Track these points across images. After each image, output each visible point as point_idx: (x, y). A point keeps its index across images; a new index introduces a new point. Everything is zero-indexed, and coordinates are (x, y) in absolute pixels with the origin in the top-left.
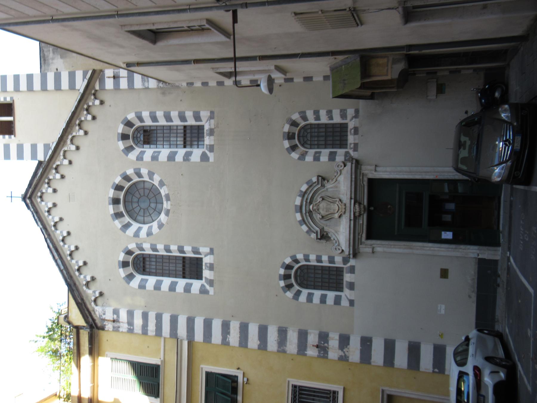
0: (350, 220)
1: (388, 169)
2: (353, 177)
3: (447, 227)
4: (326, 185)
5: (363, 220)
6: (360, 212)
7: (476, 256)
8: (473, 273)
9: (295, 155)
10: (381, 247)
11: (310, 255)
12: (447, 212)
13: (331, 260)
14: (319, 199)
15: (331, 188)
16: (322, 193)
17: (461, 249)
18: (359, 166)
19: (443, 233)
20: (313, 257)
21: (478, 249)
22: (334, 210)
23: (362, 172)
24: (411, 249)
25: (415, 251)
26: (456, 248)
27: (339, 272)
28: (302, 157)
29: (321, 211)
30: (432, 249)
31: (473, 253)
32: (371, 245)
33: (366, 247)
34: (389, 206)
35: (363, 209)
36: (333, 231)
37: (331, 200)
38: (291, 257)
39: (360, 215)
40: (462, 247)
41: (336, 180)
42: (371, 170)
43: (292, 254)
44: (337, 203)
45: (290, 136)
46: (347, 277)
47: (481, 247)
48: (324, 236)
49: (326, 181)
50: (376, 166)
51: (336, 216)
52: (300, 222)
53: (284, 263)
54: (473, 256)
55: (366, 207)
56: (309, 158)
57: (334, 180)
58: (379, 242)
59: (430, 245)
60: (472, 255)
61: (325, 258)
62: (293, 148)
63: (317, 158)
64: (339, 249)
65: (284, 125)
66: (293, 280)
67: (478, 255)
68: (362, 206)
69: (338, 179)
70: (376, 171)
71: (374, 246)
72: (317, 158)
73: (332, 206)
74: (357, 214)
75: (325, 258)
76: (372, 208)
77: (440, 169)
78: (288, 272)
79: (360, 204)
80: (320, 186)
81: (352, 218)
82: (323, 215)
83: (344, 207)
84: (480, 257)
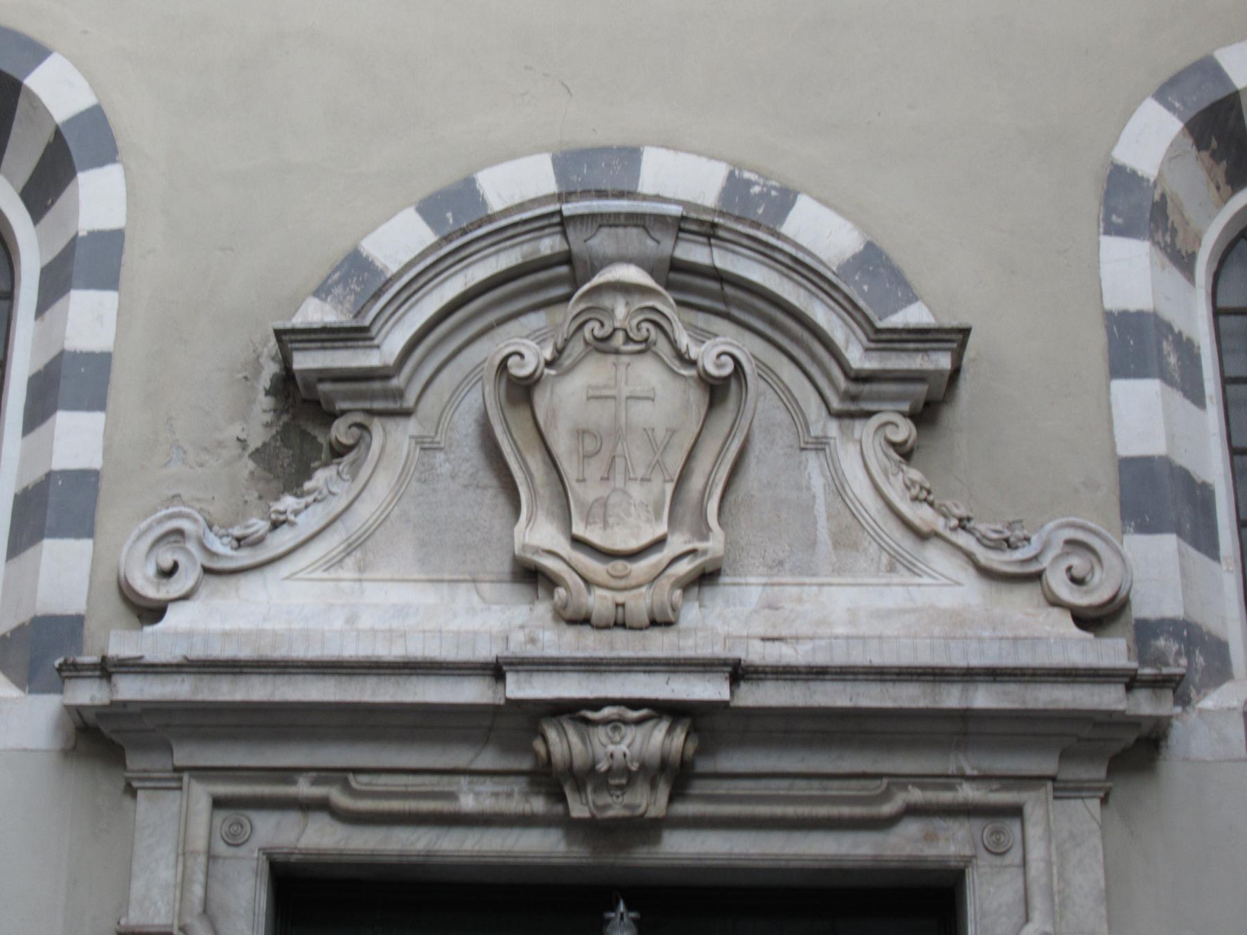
0: (496, 671)
2: (983, 698)
4: (865, 430)
6: (587, 777)
9: (1151, 139)
11: (108, 300)
15: (839, 488)
16: (784, 390)
23: (1035, 803)
28: (1133, 206)
33: (184, 853)
35: (616, 806)
36: (366, 511)
37: (709, 472)
38: (94, 119)
39: (550, 779)
41: (922, 536)
43: (122, 122)
44: (677, 544)
48: (311, 413)
49: (904, 431)
51: (539, 535)
55: (643, 856)
56: (1131, 273)
57: (922, 515)
64: (168, 573)
69: (935, 555)
72: (1136, 344)
74: (563, 743)
79: (678, 776)
80: (857, 358)
81: (519, 688)
82: (542, 400)
83: (640, 603)
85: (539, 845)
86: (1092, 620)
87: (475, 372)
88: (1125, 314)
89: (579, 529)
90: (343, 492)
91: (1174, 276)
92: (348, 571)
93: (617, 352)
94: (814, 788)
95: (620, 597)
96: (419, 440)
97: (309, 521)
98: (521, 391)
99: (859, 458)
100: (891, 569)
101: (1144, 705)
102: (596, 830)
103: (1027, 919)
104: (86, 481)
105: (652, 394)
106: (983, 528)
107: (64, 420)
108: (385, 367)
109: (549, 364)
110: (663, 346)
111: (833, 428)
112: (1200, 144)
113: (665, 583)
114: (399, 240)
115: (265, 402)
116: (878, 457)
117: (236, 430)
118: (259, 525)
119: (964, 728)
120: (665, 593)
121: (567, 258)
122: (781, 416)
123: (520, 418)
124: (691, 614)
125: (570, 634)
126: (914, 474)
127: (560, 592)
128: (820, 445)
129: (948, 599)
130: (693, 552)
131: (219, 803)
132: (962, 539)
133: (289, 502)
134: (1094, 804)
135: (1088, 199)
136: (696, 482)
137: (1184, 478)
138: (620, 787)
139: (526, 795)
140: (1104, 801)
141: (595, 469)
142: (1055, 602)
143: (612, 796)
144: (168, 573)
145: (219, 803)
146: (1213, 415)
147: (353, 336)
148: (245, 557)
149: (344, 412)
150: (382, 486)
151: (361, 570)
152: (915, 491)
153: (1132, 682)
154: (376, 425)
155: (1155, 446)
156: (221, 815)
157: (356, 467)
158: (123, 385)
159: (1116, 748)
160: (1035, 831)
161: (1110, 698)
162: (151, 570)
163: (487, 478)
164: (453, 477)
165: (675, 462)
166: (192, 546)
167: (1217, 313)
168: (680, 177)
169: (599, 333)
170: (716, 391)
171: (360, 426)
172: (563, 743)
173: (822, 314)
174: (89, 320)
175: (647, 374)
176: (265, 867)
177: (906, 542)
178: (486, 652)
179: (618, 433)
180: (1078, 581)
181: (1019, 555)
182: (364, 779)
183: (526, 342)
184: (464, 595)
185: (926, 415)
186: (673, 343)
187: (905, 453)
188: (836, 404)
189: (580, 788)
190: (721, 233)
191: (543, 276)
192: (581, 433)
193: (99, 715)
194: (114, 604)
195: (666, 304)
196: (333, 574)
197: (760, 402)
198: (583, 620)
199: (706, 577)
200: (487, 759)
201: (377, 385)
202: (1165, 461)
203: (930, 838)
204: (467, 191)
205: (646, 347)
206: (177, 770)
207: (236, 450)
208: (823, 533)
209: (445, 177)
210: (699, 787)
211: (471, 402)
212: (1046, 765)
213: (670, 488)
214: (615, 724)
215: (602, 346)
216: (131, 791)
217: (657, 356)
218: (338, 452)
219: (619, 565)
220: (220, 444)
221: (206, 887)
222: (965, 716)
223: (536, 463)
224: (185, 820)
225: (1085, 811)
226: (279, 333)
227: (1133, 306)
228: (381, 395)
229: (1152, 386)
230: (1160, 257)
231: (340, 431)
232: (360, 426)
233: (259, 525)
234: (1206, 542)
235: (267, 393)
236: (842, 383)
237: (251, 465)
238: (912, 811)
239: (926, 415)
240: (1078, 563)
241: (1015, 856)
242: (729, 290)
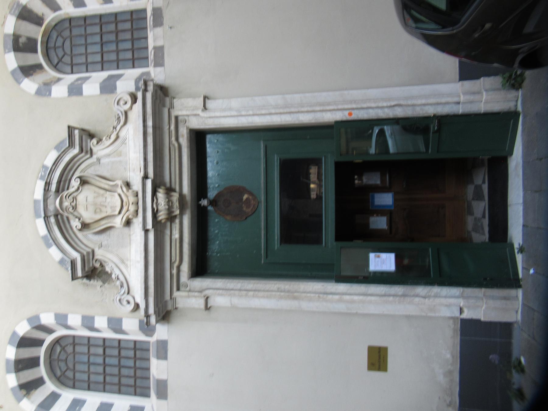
0: (146, 231)
1: (235, 103)
2: (150, 123)
3: (380, 241)
4: (95, 150)
5: (183, 230)
6: (170, 210)
7: (457, 314)
8: (449, 356)
9: (30, 85)
10: (225, 293)
11: (70, 316)
12: (381, 211)
13: (115, 324)
14: (75, 183)
15: (108, 155)
16: (87, 168)
17: (417, 296)
18: (168, 100)
19: (372, 256)
20: (74, 320)
21: (462, 296)
22: (113, 208)
23: (174, 113)
24: (295, 298)
25: (305, 305)
26: (404, 296)
27: (139, 351)
28: (45, 90)
29: (81, 210)
30: (347, 297)
31: (448, 306)
32: (201, 292)
33: (189, 297)
34: (245, 197)
35: (176, 204)
36: (115, 260)
37: (104, 184)
38: (30, 320)
39: (171, 218)
40: (421, 290)
41: (117, 137)
42: (196, 108)
43: (30, 314)
44: (119, 191)
45: (20, 45)
46: (157, 369)
47: (469, 291)
48: (93, 271)
49: (94, 141)
50: (205, 98)
51: (118, 222)
52: (44, 238)
53: (14, 334)
54: (448, 314)
55: (188, 198)
56: (59, 91)
57: (113, 137)
58: (219, 283)
59: (342, 287)
60: (446, 313)
61: (101, 322)
62: (28, 71)
63: (75, 90)
64: (128, 302)
65: (5, 18)
66: (42, 371)
67: (461, 311)
68: (175, 197)
69: (122, 134)
70: (205, 108)
71: (208, 292)
72: (75, 90)
73: (108, 200)
74: (162, 216)
75: (101, 322)
76: (204, 202)
77: (357, 94)
78: (28, 353)
79: (169, 190)
80: (76, 150)
81: (150, 226)
82: (88, 221)
83: (132, 199)
84: (466, 315)
86: (134, 99)
87: (85, 236)
88: (68, 92)
89: (117, 213)
90: (111, 264)
91: (61, 82)
92: (128, 263)
93: (76, 205)
94: (173, 161)
95: (131, 203)
96: (99, 248)
98: (85, 226)
99: (100, 150)
100: (126, 144)
101: (151, 88)
103: (199, 115)
105: (86, 196)
106: (115, 124)
107: (97, 325)
108: (81, 256)
109: (79, 219)
110: (75, 194)
111: (95, 157)
112: (32, 75)
113: (127, 194)
115: (92, 281)
116: (100, 146)
117: (98, 288)
118: (118, 283)
119: (157, 128)
120: (130, 193)
121: (56, 216)
122: (92, 168)
123: (92, 226)
126: (104, 139)
127: (130, 217)
129: (131, 132)
130: (121, 187)
131: (178, 289)
132: (118, 128)
134: (175, 100)
135: (43, 100)
136: (106, 187)
137: (105, 80)
138: (172, 203)
139: (175, 224)
140: (174, 98)
141: (104, 209)
142: (131, 108)
143: (165, 205)
144: (128, 302)
145: (178, 289)
146: (94, 75)
147: (73, 264)
149: (93, 264)
150: (110, 256)
151: (128, 260)
152: (108, 138)
153: (145, 90)
154: (96, 257)
155: (97, 86)
156: (181, 288)
157: (105, 262)
158: (89, 312)
159: (162, 95)
161: (149, 96)
162: (128, 306)
163: (108, 233)
164: (107, 240)
165: (102, 192)
166: (123, 297)
167: (72, 73)
169: (71, 208)
170: (84, 182)
171: (96, 261)
172: (162, 216)
173: (67, 159)
174: (74, 320)
175: (81, 198)
176: (192, 279)
179: (95, 204)
180: (126, 103)
181: (120, 115)
182: (173, 259)
183: (76, 224)
184: (133, 237)
185: (91, 136)
186: (73, 192)
187: (99, 141)
188: (88, 156)
189: (173, 212)
190: (48, 181)
191: (61, 221)
192: (95, 212)
193: (159, 316)
194: (136, 313)
195: (65, 193)
196: (129, 266)
197: (89, 173)
198: (137, 211)
199: (128, 185)
200: (168, 232)
201: (86, 258)
202: (100, 84)
203: (183, 136)
205: (75, 198)
206: (171, 298)
207: (103, 288)
208: (117, 159)
210: (173, 186)
211: (91, 236)
212: (166, 111)
213: (108, 193)
215: (75, 208)
216: (176, 308)
217: (77, 196)
219: (124, 204)
220: (102, 291)
221: (196, 292)
222: (154, 127)
223: (103, 222)
224: (182, 297)
225: (176, 102)
226: (73, 279)
227: (66, 90)
228: (88, 257)
230: (57, 84)
231: (97, 265)
232: (96, 261)
235: (90, 280)
236: (83, 154)
237: (106, 284)
238: (177, 139)
239: (91, 136)
240: (122, 103)
241: (186, 118)
242: (63, 179)
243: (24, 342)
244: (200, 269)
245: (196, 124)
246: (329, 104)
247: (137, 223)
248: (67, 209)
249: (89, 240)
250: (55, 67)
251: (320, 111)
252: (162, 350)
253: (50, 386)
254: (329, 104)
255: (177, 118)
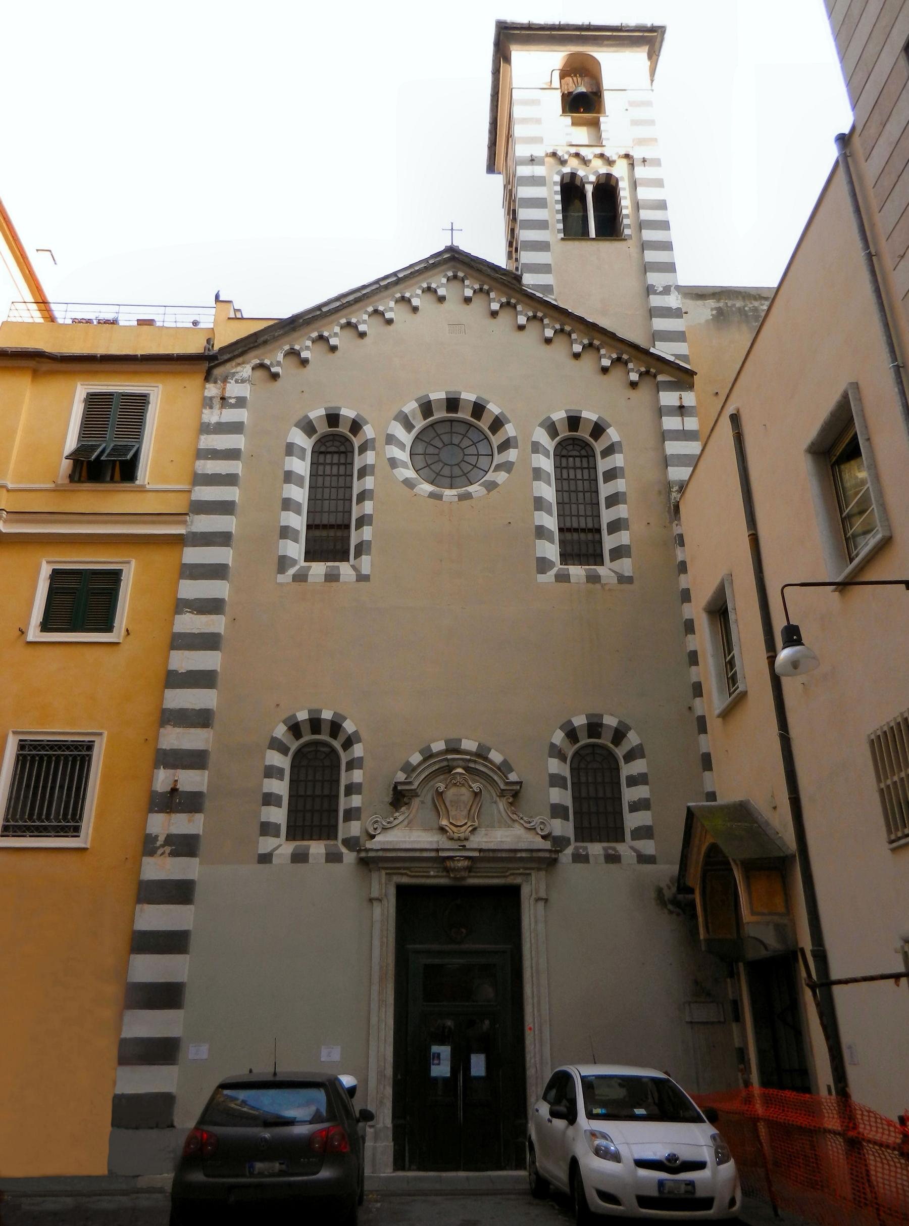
0: (437, 850)
10: (384, 914)
14: (475, 786)
25: (375, 988)
28: (556, 752)
34: (464, 930)
39: (447, 870)
41: (514, 821)
44: (469, 824)
48: (400, 798)
49: (511, 800)
51: (444, 822)
56: (554, 766)
57: (514, 817)
63: (556, 781)
64: (375, 829)
68: (464, 874)
69: (516, 825)
70: (538, 900)
71: (385, 902)
72: (556, 781)
74: (449, 864)
75: (356, 801)
79: (469, 869)
80: (502, 787)
81: (442, 854)
83: (462, 835)
85: (443, 881)
97: (401, 818)
98: (440, 794)
101: (553, 856)
102: (455, 878)
104: (358, 809)
107: (354, 797)
114: (416, 759)
124: (472, 838)
125: (450, 842)
128: (495, 802)
132: (522, 822)
133: (397, 814)
136: (472, 811)
140: (546, 871)
144: (375, 829)
146: (569, 791)
147: (410, 783)
148: (389, 826)
160: (533, 878)
165: (468, 808)
168: (469, 745)
170: (476, 795)
172: (449, 864)
174: (357, 776)
175: (463, 790)
177: (509, 822)
178: (435, 846)
187: (511, 804)
192: (451, 801)
204: (429, 748)
205: (463, 785)
209: (423, 746)
214: (458, 860)
216: (370, 871)
218: (406, 804)
225: (543, 874)
228: (414, 794)
229: (557, 789)
233: (392, 819)
234: (567, 819)
240: (542, 826)
243: (335, 727)
244: (401, 890)
245: (525, 891)
246: (539, 1010)
247: (444, 843)
248: (454, 778)
249: (427, 796)
250: (576, 754)
251: (533, 1004)
252: (333, 857)
253: (294, 746)
254: (539, 1010)
255: (530, 874)
